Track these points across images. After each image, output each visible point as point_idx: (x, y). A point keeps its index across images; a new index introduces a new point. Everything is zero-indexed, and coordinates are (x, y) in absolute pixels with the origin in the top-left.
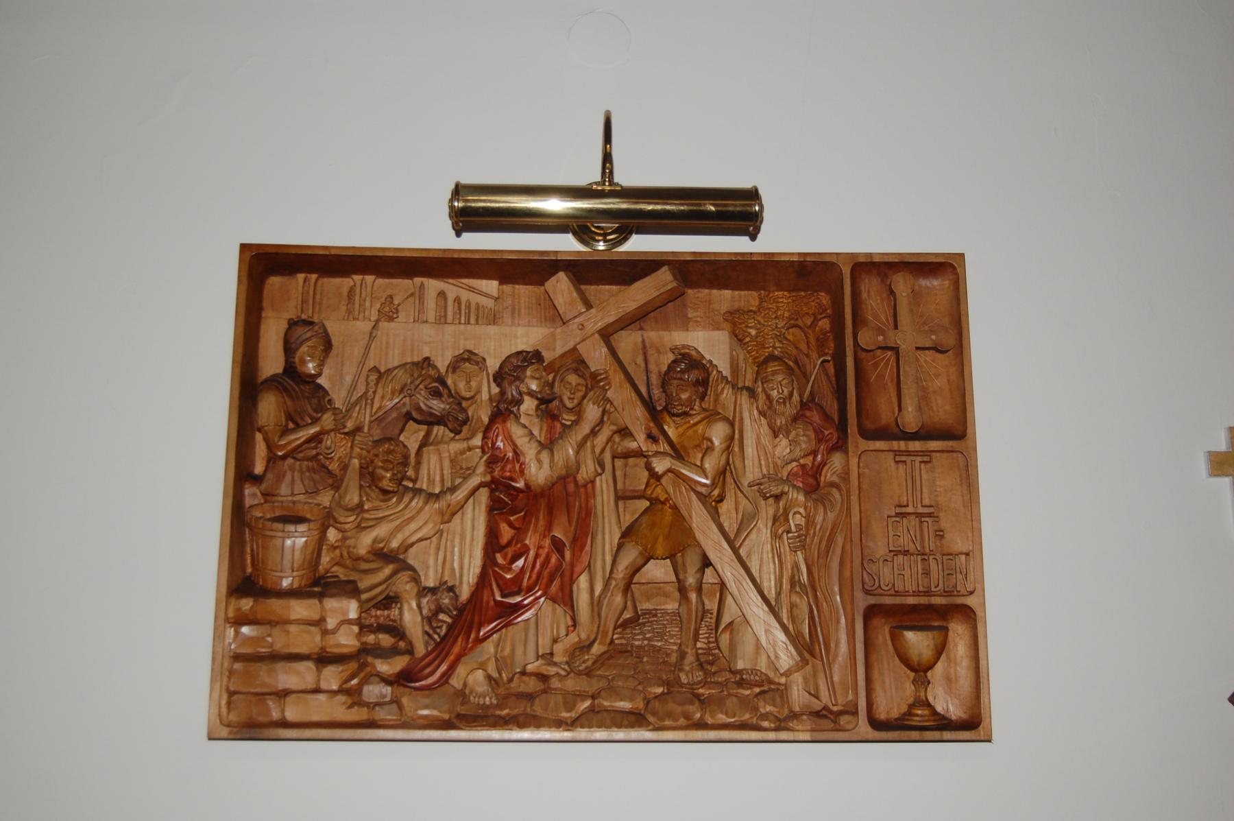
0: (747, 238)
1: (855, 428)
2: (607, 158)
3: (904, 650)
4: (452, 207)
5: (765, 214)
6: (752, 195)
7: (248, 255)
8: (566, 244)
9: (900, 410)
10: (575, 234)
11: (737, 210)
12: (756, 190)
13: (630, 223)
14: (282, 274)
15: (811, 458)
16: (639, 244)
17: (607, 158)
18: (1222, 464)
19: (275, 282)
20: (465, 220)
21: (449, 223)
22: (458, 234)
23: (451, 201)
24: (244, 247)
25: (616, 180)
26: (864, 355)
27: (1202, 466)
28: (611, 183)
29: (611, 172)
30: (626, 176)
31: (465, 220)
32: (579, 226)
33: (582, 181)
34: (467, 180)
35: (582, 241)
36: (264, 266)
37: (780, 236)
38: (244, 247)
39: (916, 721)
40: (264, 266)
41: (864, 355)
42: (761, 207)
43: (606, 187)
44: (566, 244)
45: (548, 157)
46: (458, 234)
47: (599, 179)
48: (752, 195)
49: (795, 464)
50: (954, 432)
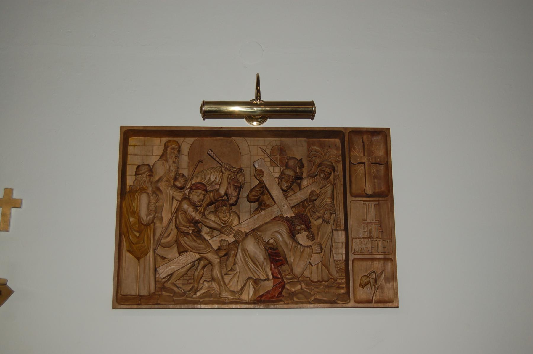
2: (258, 92)
3: (361, 277)
6: (312, 104)
7: (371, 281)
10: (246, 119)
11: (306, 110)
12: (313, 102)
13: (263, 117)
14: (345, 265)
15: (175, 201)
16: (271, 123)
17: (258, 92)
18: (10, 201)
19: (132, 141)
20: (206, 115)
22: (204, 119)
23: (201, 108)
24: (122, 127)
26: (355, 164)
28: (260, 100)
29: (260, 96)
30: (265, 97)
31: (206, 115)
32: (250, 117)
33: (248, 100)
34: (206, 100)
36: (128, 134)
37: (321, 121)
38: (122, 127)
41: (355, 164)
42: (315, 108)
43: (257, 101)
44: (243, 123)
47: (255, 98)
48: (312, 104)
49: (151, 198)
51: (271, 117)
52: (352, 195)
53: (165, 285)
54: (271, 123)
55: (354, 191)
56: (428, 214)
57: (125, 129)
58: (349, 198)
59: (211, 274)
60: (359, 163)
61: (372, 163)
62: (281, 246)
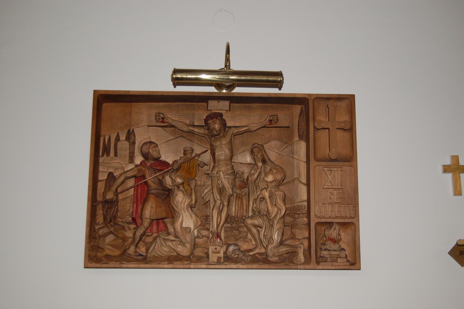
0: (278, 89)
1: (313, 158)
2: (228, 60)
3: (327, 241)
4: (172, 78)
5: (284, 81)
8: (212, 89)
9: (330, 151)
10: (215, 87)
11: (275, 79)
12: (281, 72)
16: (238, 90)
17: (228, 60)
19: (106, 106)
21: (172, 83)
22: (175, 87)
23: (172, 75)
24: (95, 92)
25: (231, 68)
26: (322, 125)
27: (440, 169)
28: (229, 69)
29: (229, 65)
30: (234, 67)
31: (176, 82)
32: (218, 85)
33: (217, 68)
34: (178, 67)
35: (217, 89)
36: (102, 100)
37: (288, 89)
38: (95, 92)
39: (148, 231)
40: (102, 100)
41: (322, 125)
43: (227, 70)
44: (212, 89)
45: (207, 59)
46: (175, 87)
47: (224, 67)
48: (279, 74)
50: (349, 158)
51: (239, 86)
52: (317, 160)
53: (184, 226)
54: (238, 90)
55: (319, 155)
56: (390, 184)
57: (99, 96)
58: (313, 163)
59: (272, 182)
60: (323, 128)
61: (337, 129)
62: (189, 264)
